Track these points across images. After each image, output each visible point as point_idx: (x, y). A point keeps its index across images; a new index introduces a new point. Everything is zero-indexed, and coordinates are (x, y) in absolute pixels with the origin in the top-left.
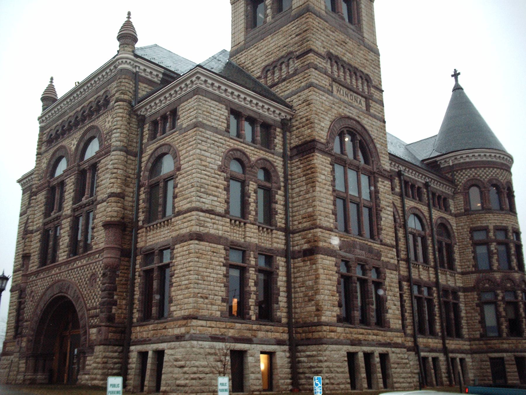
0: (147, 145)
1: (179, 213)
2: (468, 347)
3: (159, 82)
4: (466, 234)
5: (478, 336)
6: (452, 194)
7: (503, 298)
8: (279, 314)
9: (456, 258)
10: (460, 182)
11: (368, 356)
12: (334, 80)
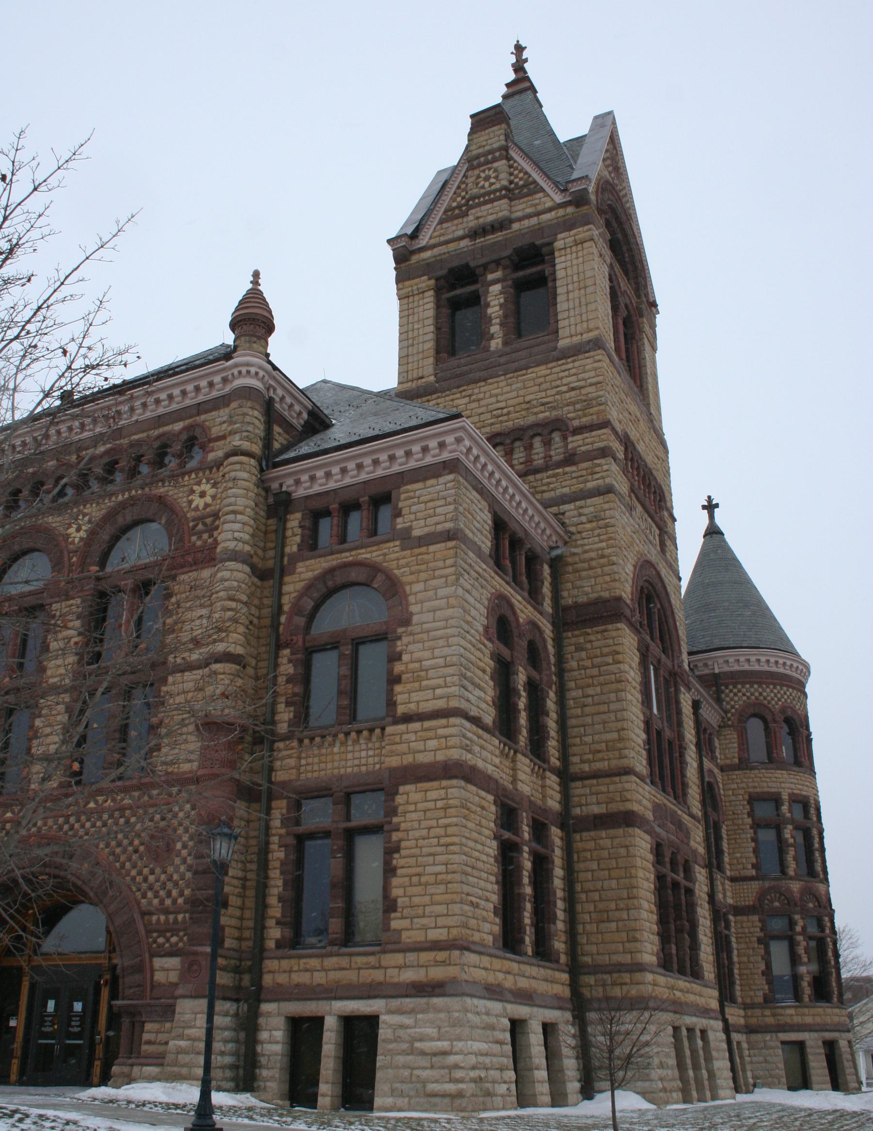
0: (295, 559)
1: (408, 718)
2: (742, 1021)
3: (300, 428)
5: (761, 1000)
7: (804, 928)
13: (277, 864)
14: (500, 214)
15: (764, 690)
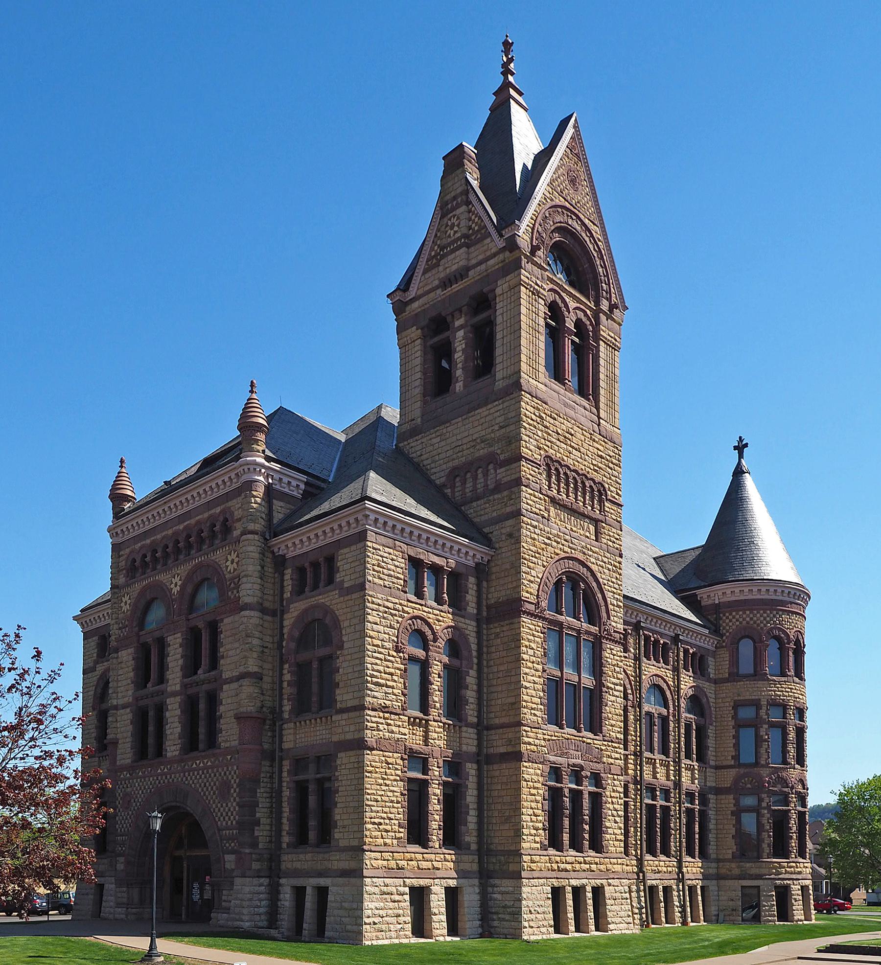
0: (290, 601)
4: (728, 712)
6: (714, 649)
8: (467, 839)
9: (710, 745)
10: (727, 631)
11: (578, 892)
12: (553, 500)
13: (286, 799)
14: (461, 263)
15: (755, 615)
